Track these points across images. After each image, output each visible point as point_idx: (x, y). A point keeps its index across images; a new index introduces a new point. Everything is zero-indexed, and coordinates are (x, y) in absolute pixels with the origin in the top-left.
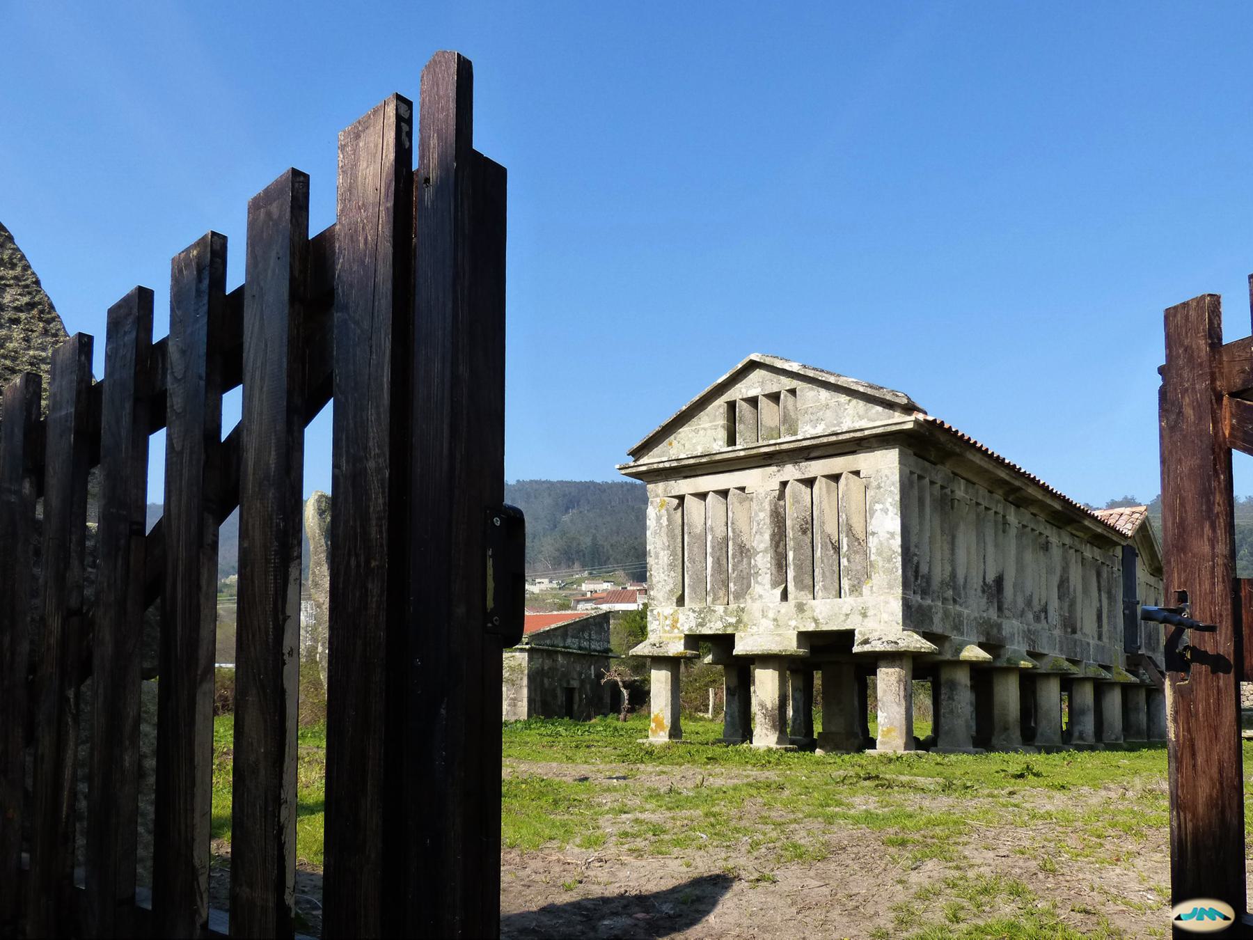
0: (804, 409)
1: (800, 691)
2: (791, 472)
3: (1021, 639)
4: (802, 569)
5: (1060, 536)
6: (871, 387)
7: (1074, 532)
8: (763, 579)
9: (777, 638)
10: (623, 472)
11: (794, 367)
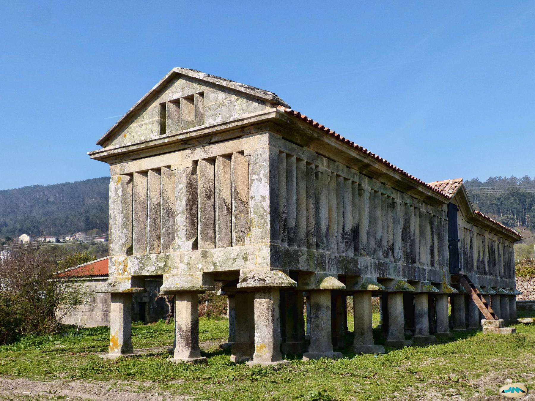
2: (199, 153)
3: (373, 269)
4: (207, 225)
5: (402, 198)
6: (250, 88)
7: (413, 195)
8: (181, 233)
9: (189, 278)
10: (92, 157)
11: (201, 76)
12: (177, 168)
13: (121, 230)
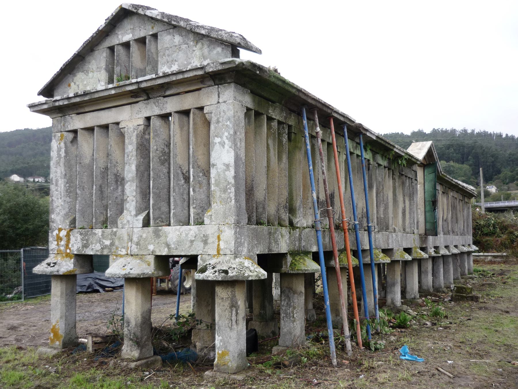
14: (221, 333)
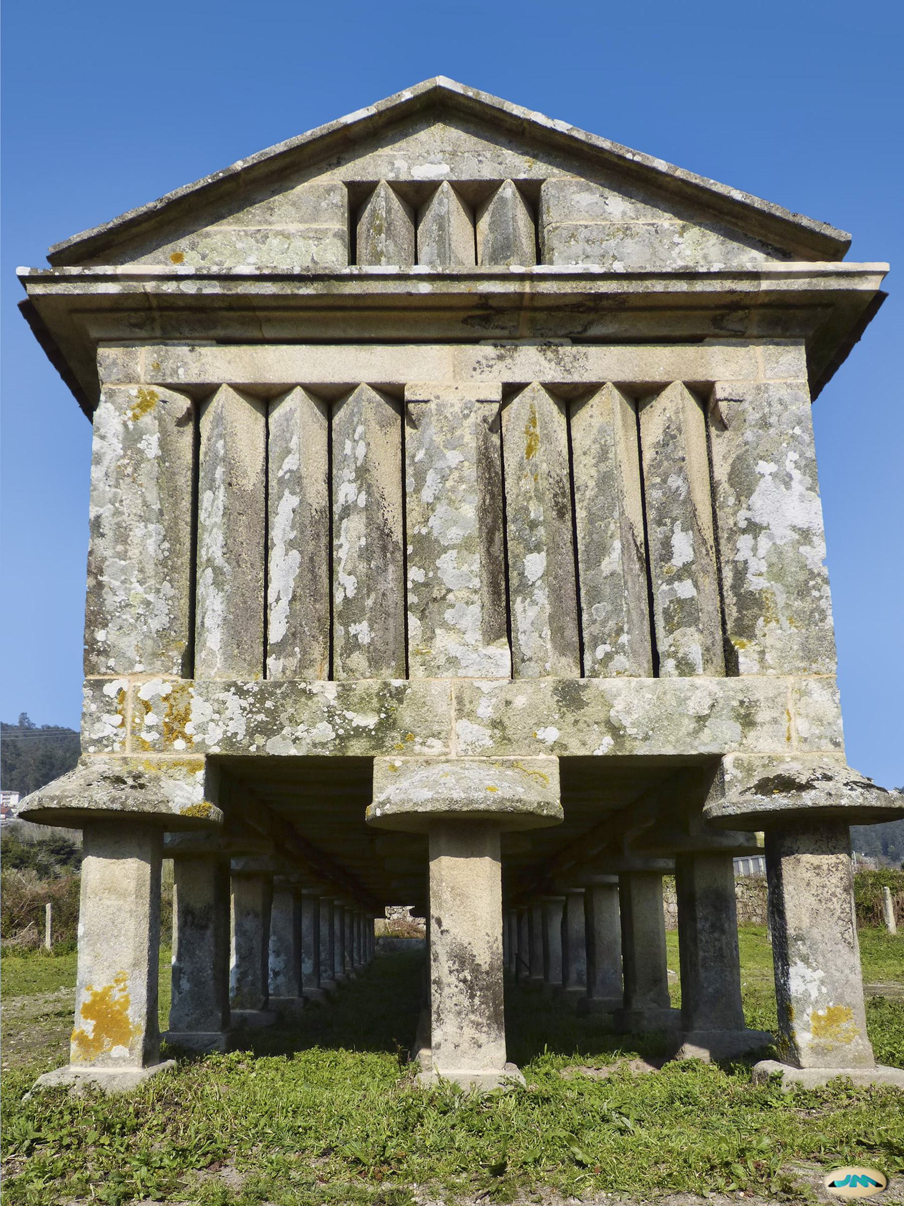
0: (567, 229)
1: (256, 915)
12: (438, 397)
13: (151, 582)
14: (820, 959)
